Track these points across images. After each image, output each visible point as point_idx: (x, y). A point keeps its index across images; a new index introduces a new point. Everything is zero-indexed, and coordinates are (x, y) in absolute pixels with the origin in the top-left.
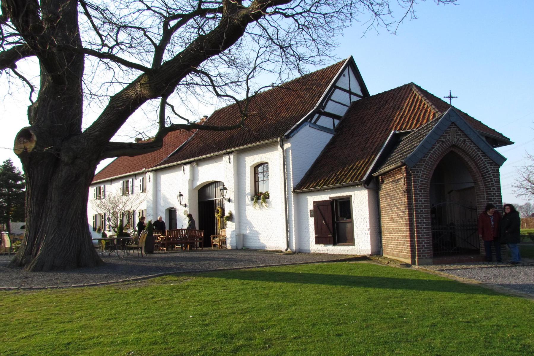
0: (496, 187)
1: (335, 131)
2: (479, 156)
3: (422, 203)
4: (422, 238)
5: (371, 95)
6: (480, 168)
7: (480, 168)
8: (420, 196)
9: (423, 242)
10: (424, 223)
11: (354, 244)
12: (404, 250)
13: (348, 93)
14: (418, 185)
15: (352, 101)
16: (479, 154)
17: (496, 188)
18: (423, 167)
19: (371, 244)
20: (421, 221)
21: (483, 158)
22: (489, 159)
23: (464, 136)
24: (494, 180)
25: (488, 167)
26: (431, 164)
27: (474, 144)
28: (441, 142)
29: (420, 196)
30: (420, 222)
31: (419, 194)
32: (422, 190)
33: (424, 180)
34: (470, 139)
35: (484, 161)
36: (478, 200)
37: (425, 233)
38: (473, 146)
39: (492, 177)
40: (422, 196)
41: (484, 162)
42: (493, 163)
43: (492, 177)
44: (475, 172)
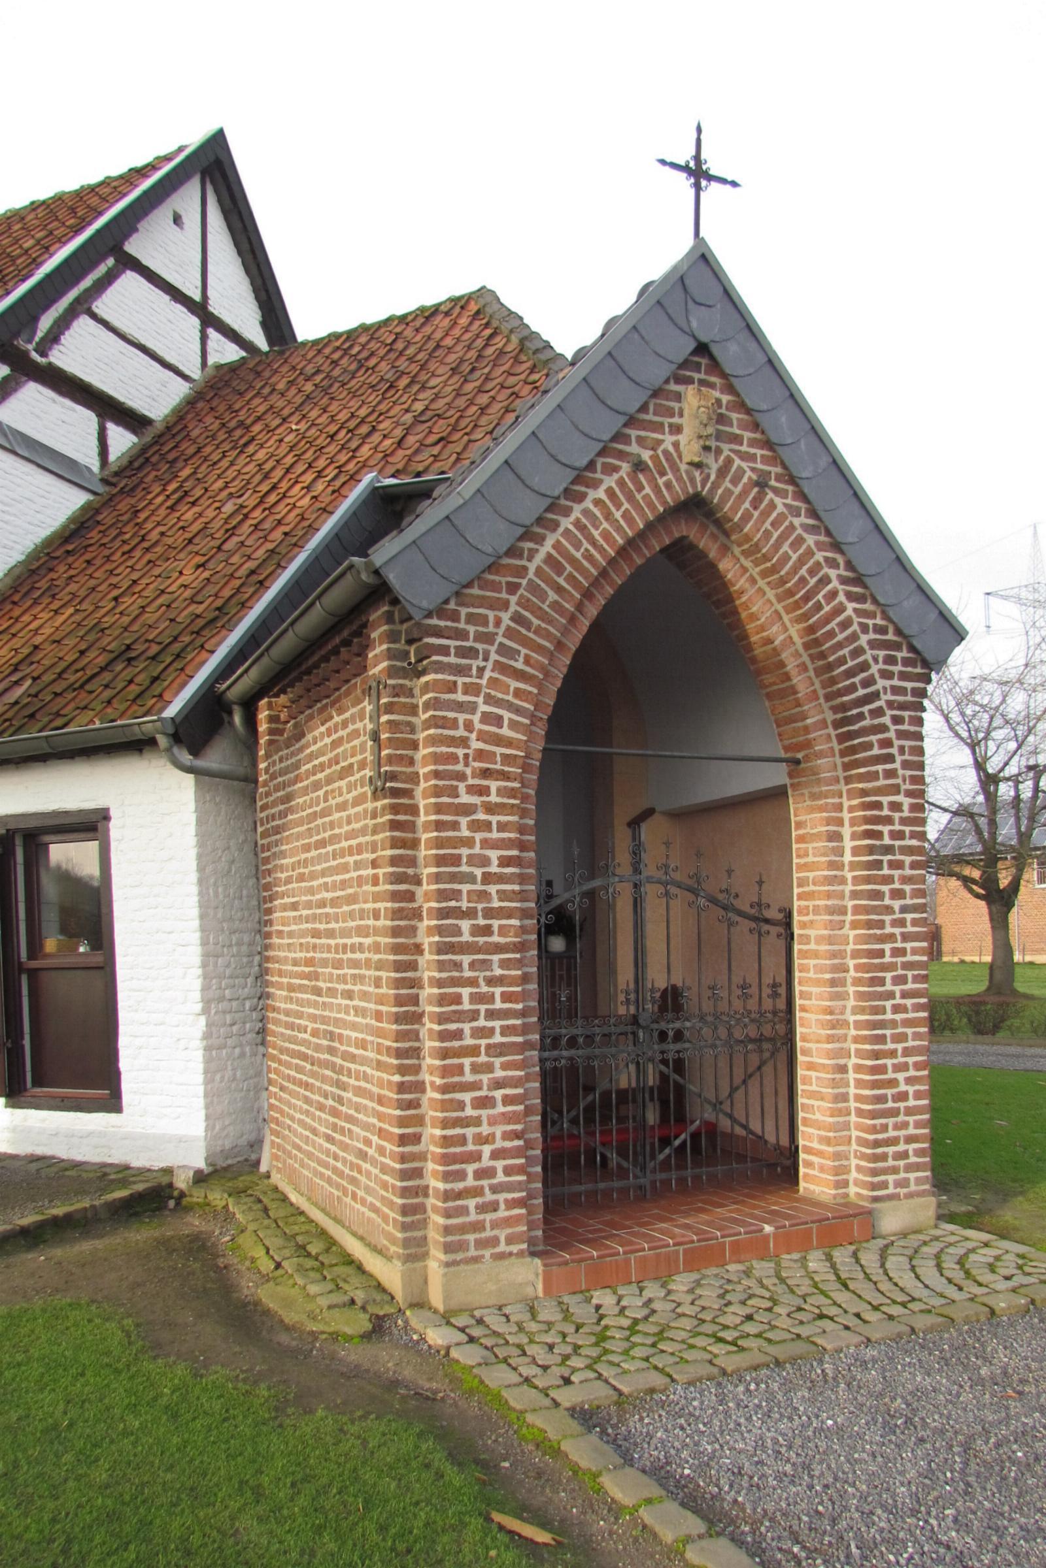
0: (909, 794)
1: (105, 481)
2: (833, 594)
3: (488, 878)
4: (477, 1122)
5: (300, 339)
6: (830, 667)
7: (830, 667)
8: (476, 826)
9: (487, 1150)
10: (491, 1015)
11: (113, 1103)
12: (368, 1190)
13: (192, 312)
14: (464, 742)
15: (211, 361)
16: (835, 584)
17: (906, 802)
18: (506, 617)
19: (211, 1097)
20: (477, 998)
21: (850, 606)
22: (879, 621)
23: (759, 452)
24: (902, 750)
25: (874, 669)
26: (555, 605)
27: (813, 513)
28: (625, 467)
29: (476, 826)
30: (466, 1006)
31: (468, 810)
32: (494, 785)
33: (507, 715)
34: (792, 480)
35: (855, 627)
36: (801, 867)
37: (498, 1084)
38: (806, 527)
39: (892, 734)
40: (488, 826)
41: (854, 637)
42: (897, 646)
43: (892, 734)
44: (803, 690)
